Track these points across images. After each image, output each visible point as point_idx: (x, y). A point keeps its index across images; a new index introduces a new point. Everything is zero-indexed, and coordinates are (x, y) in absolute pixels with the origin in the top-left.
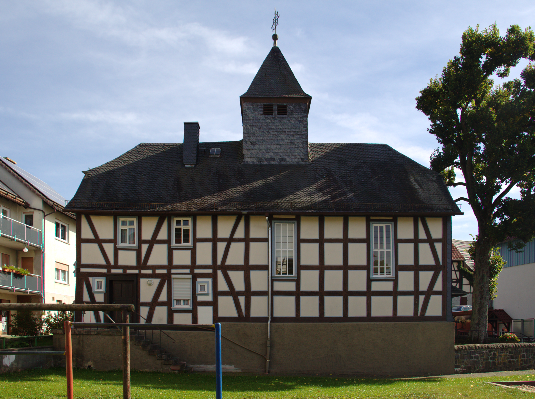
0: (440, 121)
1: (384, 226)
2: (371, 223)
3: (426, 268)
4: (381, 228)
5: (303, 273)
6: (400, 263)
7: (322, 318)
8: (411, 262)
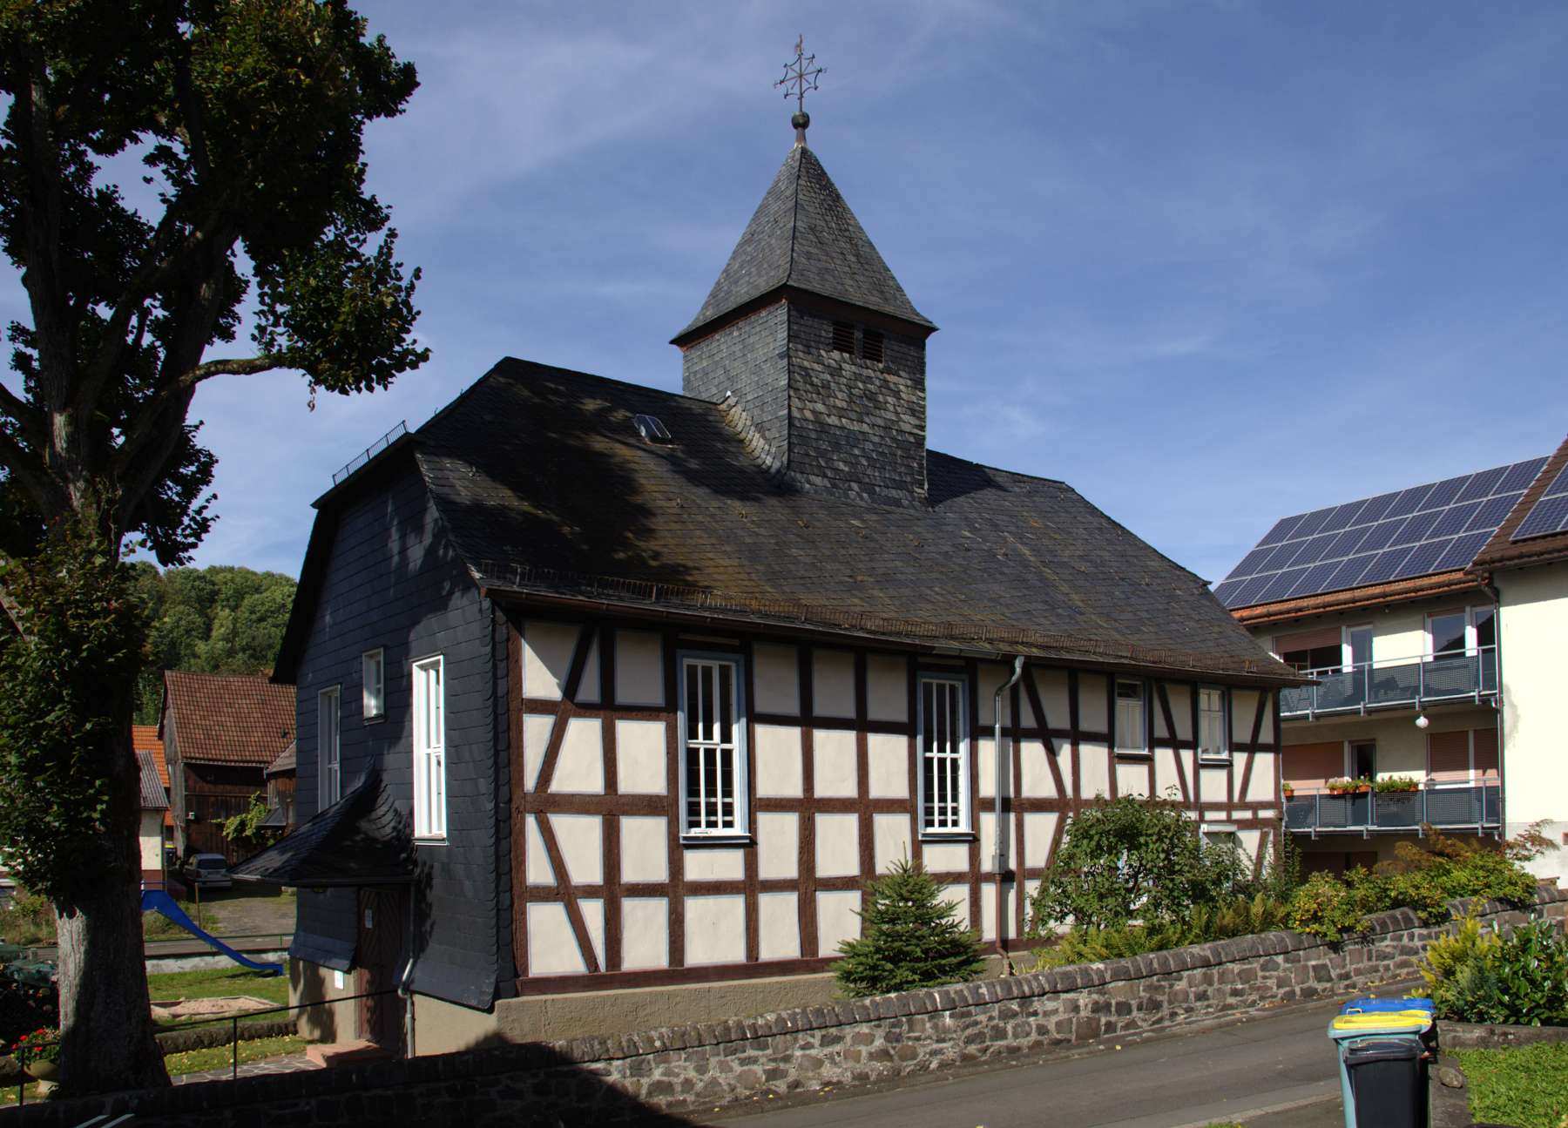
0: (348, 166)
1: (715, 666)
2: (679, 652)
3: (577, 804)
4: (707, 672)
5: (764, 819)
6: (763, 791)
7: (677, 972)
8: (847, 788)
